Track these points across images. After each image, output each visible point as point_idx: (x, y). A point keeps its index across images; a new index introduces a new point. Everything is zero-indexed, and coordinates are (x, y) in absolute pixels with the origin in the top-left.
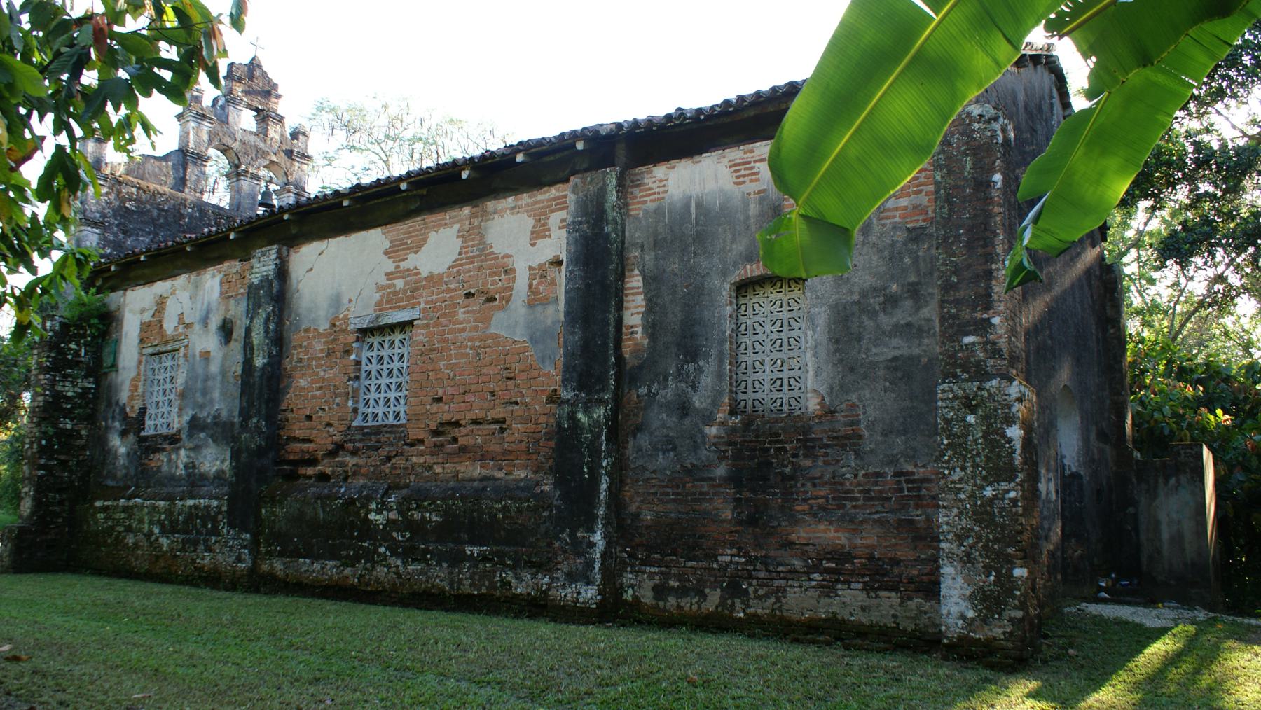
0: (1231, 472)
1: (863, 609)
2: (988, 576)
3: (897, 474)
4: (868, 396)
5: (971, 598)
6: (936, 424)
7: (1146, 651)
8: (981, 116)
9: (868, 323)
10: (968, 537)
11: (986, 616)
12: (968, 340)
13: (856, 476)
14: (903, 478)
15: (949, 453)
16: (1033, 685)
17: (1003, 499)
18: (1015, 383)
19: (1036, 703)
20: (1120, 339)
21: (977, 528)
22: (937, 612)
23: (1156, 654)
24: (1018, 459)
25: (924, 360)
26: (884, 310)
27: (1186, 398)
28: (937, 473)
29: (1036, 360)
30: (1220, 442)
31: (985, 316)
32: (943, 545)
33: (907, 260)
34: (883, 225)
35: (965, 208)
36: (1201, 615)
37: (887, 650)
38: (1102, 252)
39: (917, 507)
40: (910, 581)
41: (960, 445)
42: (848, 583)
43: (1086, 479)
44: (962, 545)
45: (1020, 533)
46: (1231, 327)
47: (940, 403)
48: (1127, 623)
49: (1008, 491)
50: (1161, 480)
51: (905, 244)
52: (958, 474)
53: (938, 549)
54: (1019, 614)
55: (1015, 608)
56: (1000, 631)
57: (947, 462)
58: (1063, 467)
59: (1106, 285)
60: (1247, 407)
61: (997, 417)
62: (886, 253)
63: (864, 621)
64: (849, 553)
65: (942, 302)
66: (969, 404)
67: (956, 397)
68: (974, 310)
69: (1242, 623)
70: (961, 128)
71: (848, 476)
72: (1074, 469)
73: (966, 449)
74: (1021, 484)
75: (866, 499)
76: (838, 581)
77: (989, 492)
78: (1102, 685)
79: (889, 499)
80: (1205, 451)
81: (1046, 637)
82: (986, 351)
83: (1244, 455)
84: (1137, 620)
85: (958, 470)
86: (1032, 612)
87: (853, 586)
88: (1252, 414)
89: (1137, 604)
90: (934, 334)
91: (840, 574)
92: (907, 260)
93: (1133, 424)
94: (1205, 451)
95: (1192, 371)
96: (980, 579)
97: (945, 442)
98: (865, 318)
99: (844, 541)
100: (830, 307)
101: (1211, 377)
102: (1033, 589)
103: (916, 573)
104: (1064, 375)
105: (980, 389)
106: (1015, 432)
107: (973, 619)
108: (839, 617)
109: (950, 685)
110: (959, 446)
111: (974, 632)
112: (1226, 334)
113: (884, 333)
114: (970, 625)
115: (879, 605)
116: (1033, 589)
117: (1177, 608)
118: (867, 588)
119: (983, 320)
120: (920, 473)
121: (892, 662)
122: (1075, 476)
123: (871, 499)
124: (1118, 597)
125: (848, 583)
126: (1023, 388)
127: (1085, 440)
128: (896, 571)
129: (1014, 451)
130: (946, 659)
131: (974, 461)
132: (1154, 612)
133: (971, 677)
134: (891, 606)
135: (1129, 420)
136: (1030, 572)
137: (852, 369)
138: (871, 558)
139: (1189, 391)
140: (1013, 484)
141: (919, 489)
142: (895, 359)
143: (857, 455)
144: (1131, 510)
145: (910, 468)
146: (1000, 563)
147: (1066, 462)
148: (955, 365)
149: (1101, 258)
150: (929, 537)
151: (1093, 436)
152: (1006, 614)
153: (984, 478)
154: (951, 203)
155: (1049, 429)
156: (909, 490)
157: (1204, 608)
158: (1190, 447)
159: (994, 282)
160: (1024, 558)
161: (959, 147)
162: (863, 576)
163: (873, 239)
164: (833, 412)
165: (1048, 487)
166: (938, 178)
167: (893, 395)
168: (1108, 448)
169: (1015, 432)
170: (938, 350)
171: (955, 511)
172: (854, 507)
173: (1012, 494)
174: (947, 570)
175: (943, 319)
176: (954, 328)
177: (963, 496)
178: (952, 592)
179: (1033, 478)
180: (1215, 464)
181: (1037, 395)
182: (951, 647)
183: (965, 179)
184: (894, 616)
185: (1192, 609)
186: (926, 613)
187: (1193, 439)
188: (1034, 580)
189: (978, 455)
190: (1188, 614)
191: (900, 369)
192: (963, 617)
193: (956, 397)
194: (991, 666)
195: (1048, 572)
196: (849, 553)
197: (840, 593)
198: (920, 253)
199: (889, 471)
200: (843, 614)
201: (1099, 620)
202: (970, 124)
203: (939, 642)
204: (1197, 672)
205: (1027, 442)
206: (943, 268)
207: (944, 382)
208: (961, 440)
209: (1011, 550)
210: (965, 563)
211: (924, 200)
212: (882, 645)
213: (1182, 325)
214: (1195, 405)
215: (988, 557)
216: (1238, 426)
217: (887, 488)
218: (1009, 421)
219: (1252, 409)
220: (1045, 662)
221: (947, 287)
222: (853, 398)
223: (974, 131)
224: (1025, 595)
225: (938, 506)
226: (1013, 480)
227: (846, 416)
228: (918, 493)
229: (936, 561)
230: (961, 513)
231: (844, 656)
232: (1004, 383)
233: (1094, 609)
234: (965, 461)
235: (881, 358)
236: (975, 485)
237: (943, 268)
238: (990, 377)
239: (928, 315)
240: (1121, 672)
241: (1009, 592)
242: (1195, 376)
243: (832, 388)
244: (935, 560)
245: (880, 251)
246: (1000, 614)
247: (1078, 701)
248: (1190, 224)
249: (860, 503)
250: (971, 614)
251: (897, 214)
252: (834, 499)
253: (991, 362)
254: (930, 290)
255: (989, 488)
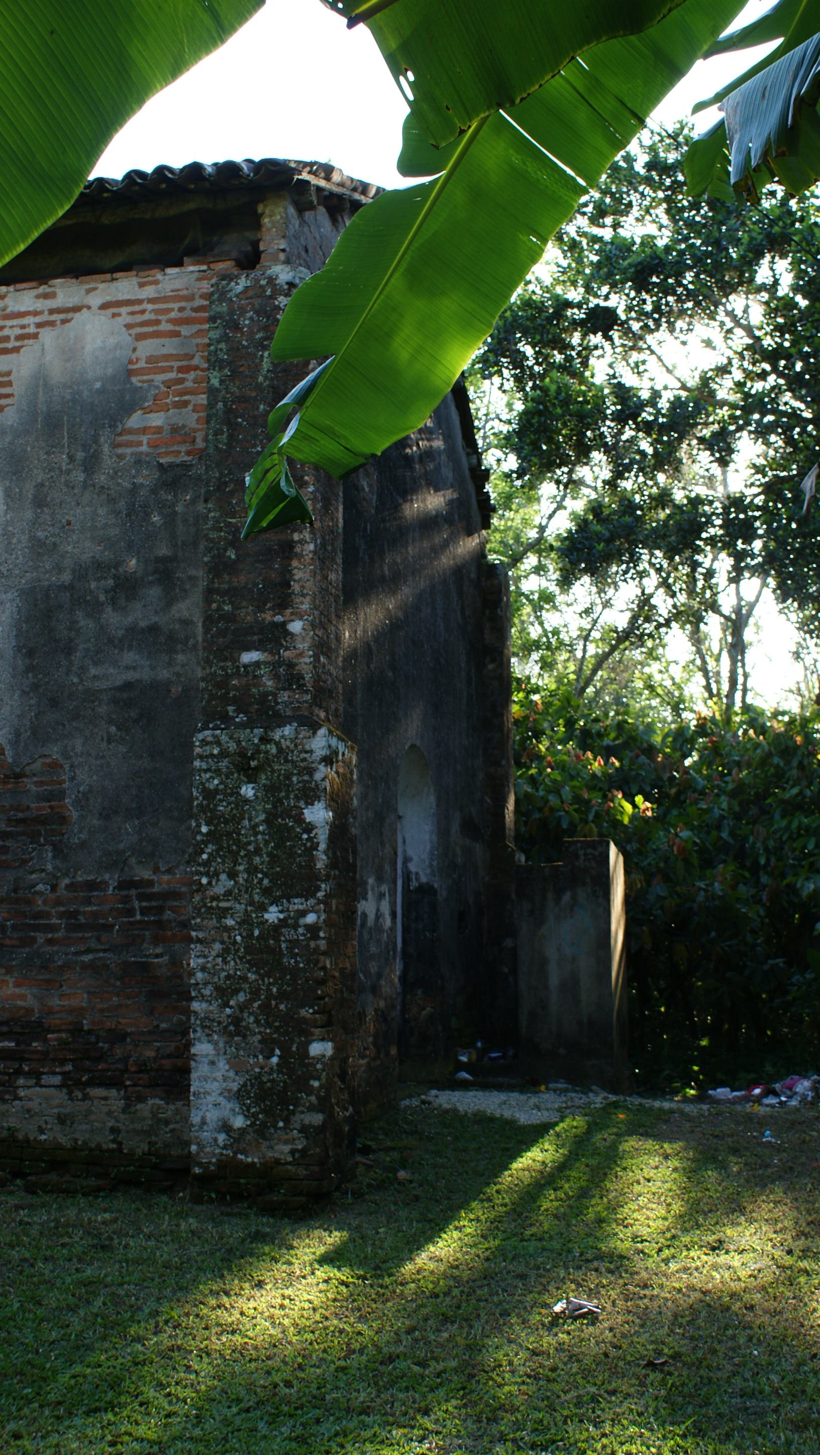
0: (649, 883)
1: (62, 1120)
2: (268, 1057)
3: (124, 885)
4: (79, 748)
5: (239, 1095)
6: (192, 799)
7: (515, 1165)
8: (291, 285)
9: (85, 623)
10: (237, 991)
11: (264, 1124)
12: (249, 657)
13: (54, 888)
14: (133, 892)
15: (210, 848)
16: (334, 1238)
17: (296, 926)
18: (322, 731)
19: (334, 1273)
20: (505, 683)
21: (252, 976)
22: (186, 1119)
23: (528, 1169)
24: (321, 860)
25: (176, 690)
26: (113, 602)
27: (594, 775)
28: (191, 883)
29: (364, 701)
30: (635, 841)
31: (279, 618)
32: (196, 1006)
33: (156, 518)
34: (121, 457)
35: (255, 437)
36: (598, 1099)
37: (100, 1189)
38: (483, 545)
39: (156, 940)
40: (143, 1067)
41: (229, 834)
42: (36, 1075)
43: (442, 894)
44: (226, 1005)
45: (322, 982)
46: (657, 677)
47: (197, 763)
48: (492, 1119)
49: (303, 913)
50: (550, 895)
51: (154, 491)
52: (224, 883)
53: (188, 1012)
54: (317, 1119)
55: (312, 1109)
56: (287, 1148)
57: (206, 864)
58: (407, 876)
59: (484, 601)
60: (673, 791)
61: (290, 788)
62: (122, 504)
63: (63, 1140)
64: (39, 1024)
65: (209, 592)
66: (245, 766)
67: (224, 754)
68: (261, 609)
69: (651, 1109)
70: (257, 302)
71: (40, 887)
72: (424, 879)
73: (238, 842)
74: (326, 901)
75: (71, 928)
76: (19, 1072)
77: (273, 915)
78: (442, 1230)
79: (109, 927)
80: (613, 849)
81: (366, 1150)
82: (276, 677)
83: (667, 860)
84: (507, 1114)
85: (223, 877)
86: (341, 1114)
87: (45, 1080)
88: (678, 801)
89: (511, 1088)
90: (195, 646)
91: (23, 1060)
92: (156, 518)
93: (517, 811)
94: (613, 849)
95: (600, 735)
96: (254, 1063)
97: (204, 829)
98: (80, 614)
99: (30, 1002)
100: (23, 593)
101: (626, 745)
102: (343, 1076)
103: (150, 1053)
104: (412, 728)
105: (264, 740)
106: (318, 814)
107: (243, 1131)
108: (20, 1136)
109: (193, 1251)
110: (226, 837)
111: (244, 1152)
112: (651, 688)
113: (111, 641)
114: (237, 1140)
115: (89, 1113)
116: (343, 1076)
117: (566, 1091)
118: (70, 1084)
119: (275, 625)
120: (163, 882)
121: (100, 1215)
122: (426, 890)
123: (79, 927)
124: (484, 1080)
125: (36, 1075)
126: (334, 742)
127: (443, 833)
128: (119, 1052)
129: (315, 847)
130: (197, 1200)
131: (250, 863)
132: (534, 1100)
133: (234, 1231)
134: (109, 1113)
135: (511, 805)
136: (338, 1049)
137: (54, 703)
138: (77, 1030)
139: (596, 766)
140: (311, 902)
141: (160, 910)
142: (128, 686)
143: (59, 851)
144: (509, 942)
145: (147, 874)
146: (289, 1034)
147: (412, 867)
148: (225, 700)
149: (481, 554)
150: (173, 991)
151: (455, 827)
152: (300, 1119)
153: (266, 892)
154: (233, 426)
155: (384, 816)
156: (143, 911)
157: (603, 1087)
158: (593, 845)
159: (295, 563)
160: (328, 1024)
161: (251, 333)
162: (63, 1062)
163: (101, 479)
164: (18, 776)
165: (377, 908)
166: (215, 382)
167: (122, 749)
168: (478, 848)
169: (318, 814)
170: (200, 673)
171: (217, 947)
172: (50, 942)
173: (311, 918)
174: (202, 1048)
175: (209, 620)
176: (228, 638)
177: (230, 922)
178: (209, 1086)
179: (349, 889)
180: (627, 872)
181: (363, 755)
182: (206, 1180)
183: (259, 387)
184: (113, 1130)
185: (586, 1091)
186: (167, 1122)
187: (601, 835)
188: (345, 1060)
189: (258, 851)
190: (579, 1099)
191: (138, 706)
192: (226, 1127)
193: (224, 754)
194: (270, 1210)
195: (375, 1043)
196: (39, 1024)
197: (21, 1093)
198: (179, 509)
199: (112, 879)
200: (27, 1130)
201: (451, 1118)
202: (272, 297)
203: (187, 1171)
204: (584, 1194)
205: (338, 831)
206: (213, 535)
207: (205, 728)
208: (230, 827)
209: (306, 1013)
210: (231, 1035)
211: (190, 419)
212: (92, 1182)
213: (594, 672)
214: (606, 787)
215: (268, 1025)
216: (660, 819)
217: (107, 908)
218: (310, 795)
219: (679, 793)
220: (358, 1195)
221: (219, 567)
222: (54, 751)
223: (278, 308)
224: (328, 1087)
225: (190, 940)
226: (313, 894)
227: (41, 784)
228: (160, 917)
229: (185, 1033)
230: (226, 951)
231: (18, 1207)
232: (304, 732)
233: (445, 1099)
234: (236, 863)
235: (104, 685)
236: (251, 903)
237: (213, 535)
238: (282, 721)
239: (186, 614)
240: (474, 1204)
241: (302, 1084)
242: (606, 741)
243: (18, 734)
244: (182, 1033)
245: (111, 501)
246: (287, 1121)
247: (401, 1262)
248: (606, 512)
249: (59, 935)
250: (239, 1122)
251: (144, 439)
252: (14, 927)
253: (284, 696)
254: (193, 572)
255: (273, 909)
